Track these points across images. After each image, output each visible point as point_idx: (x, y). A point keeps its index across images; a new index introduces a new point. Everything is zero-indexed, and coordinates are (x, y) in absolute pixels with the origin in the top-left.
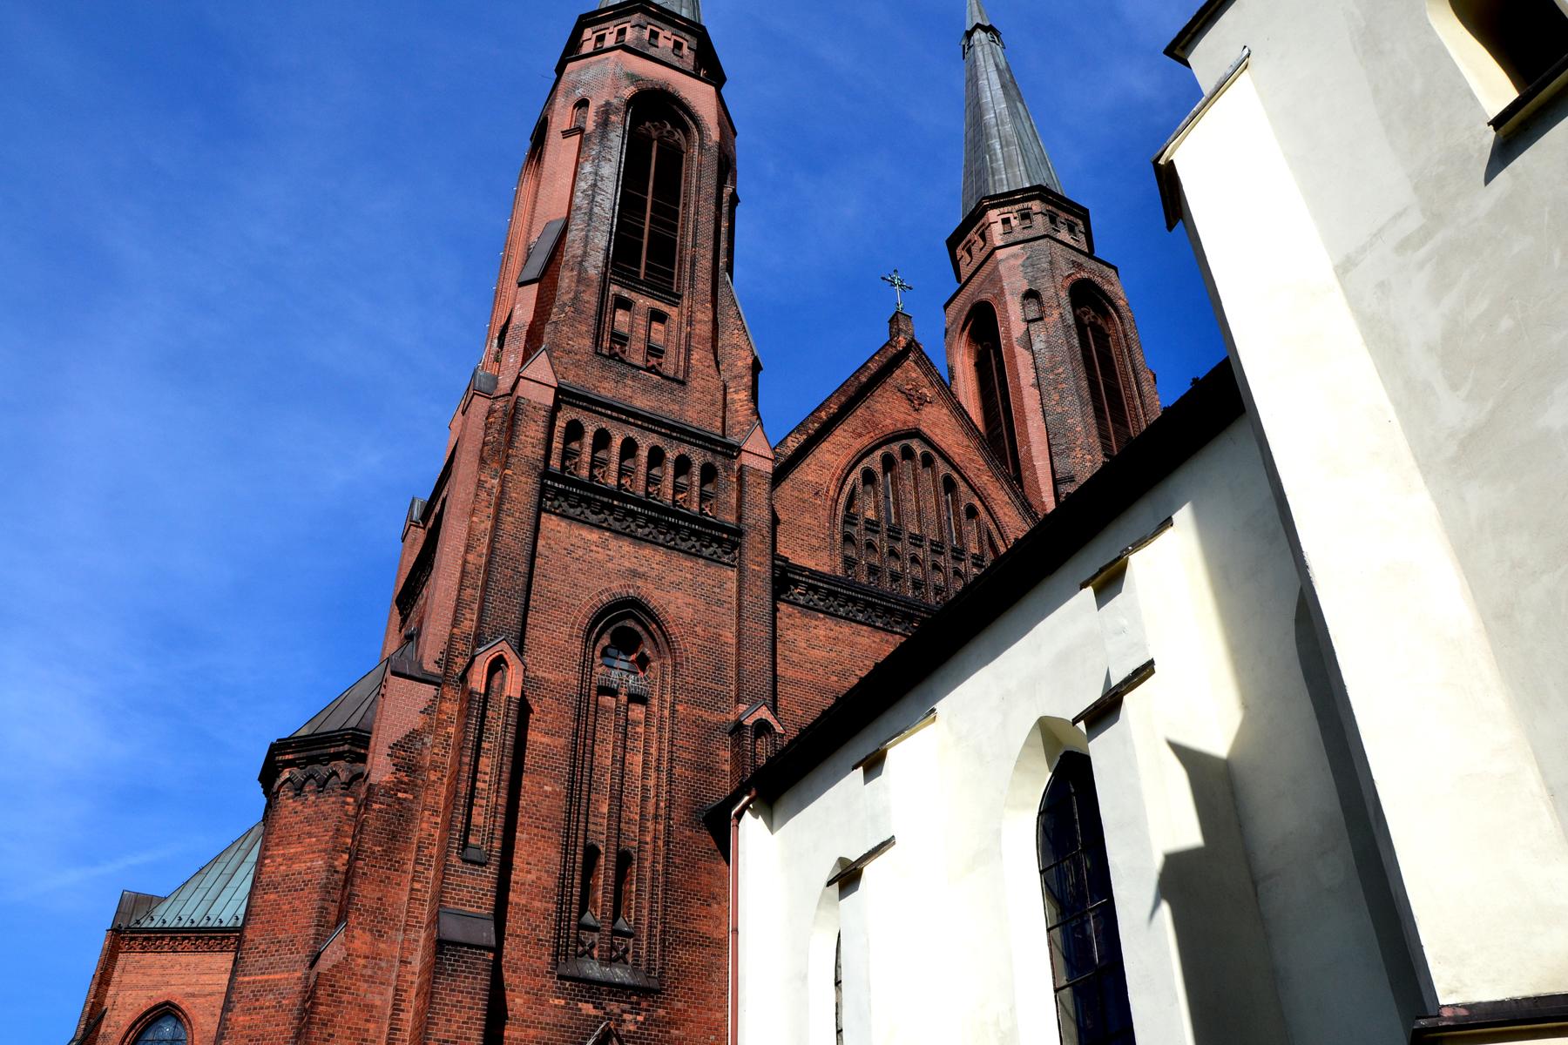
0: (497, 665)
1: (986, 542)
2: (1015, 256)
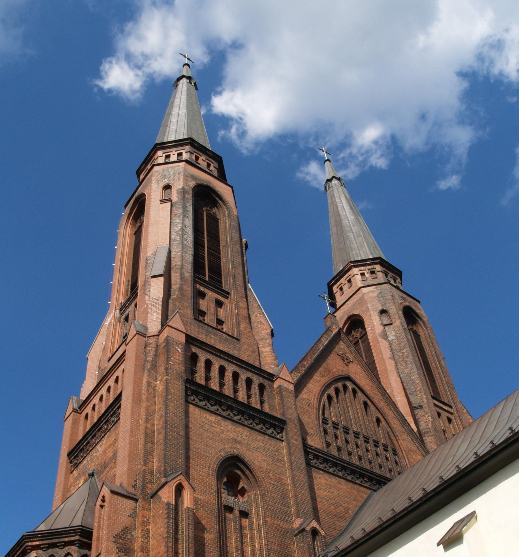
0: (179, 489)
1: (387, 437)
2: (372, 291)
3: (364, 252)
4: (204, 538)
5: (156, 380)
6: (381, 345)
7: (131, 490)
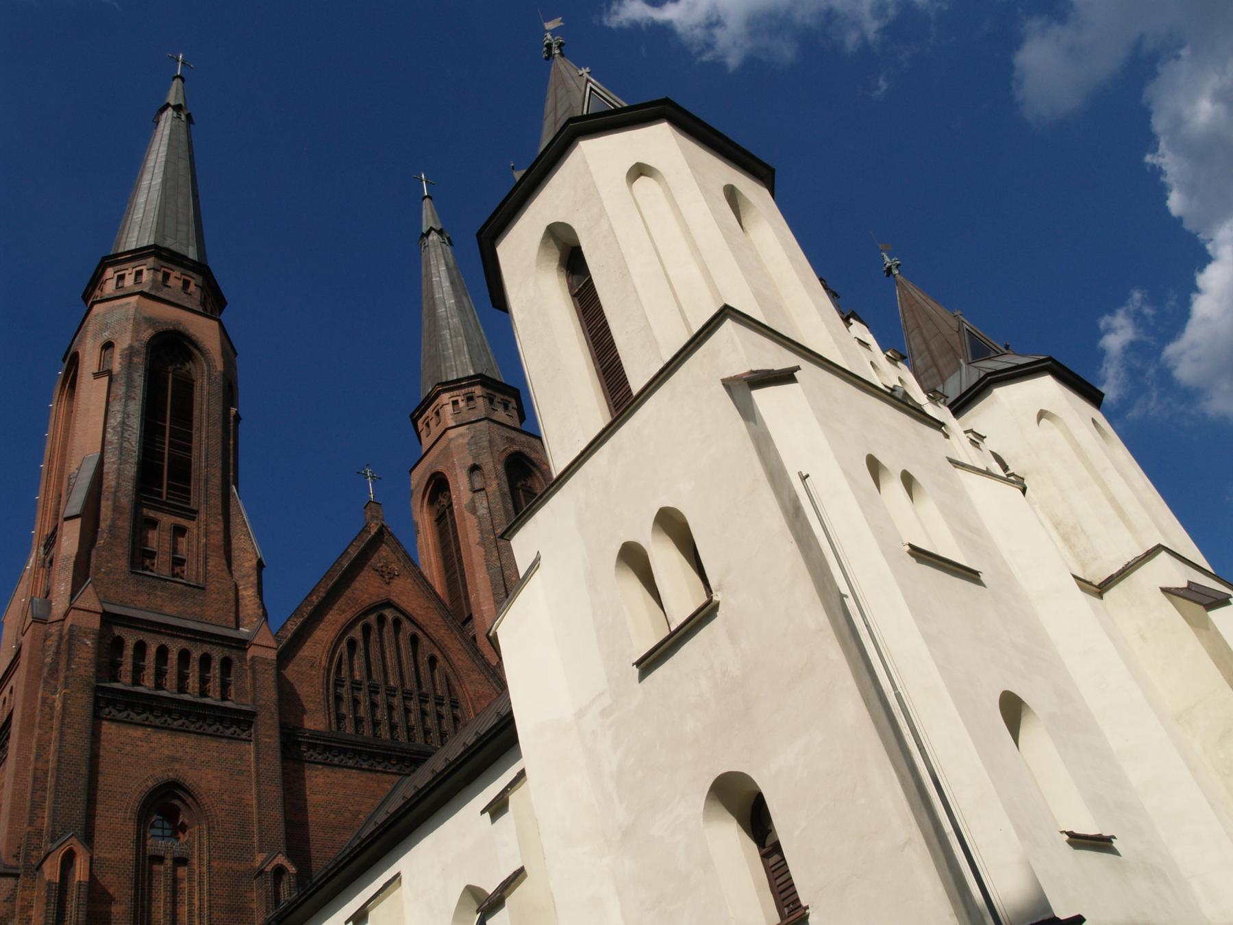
2: (462, 435)
3: (462, 362)
4: (109, 913)
5: (55, 693)
6: (468, 524)
7: (13, 862)
